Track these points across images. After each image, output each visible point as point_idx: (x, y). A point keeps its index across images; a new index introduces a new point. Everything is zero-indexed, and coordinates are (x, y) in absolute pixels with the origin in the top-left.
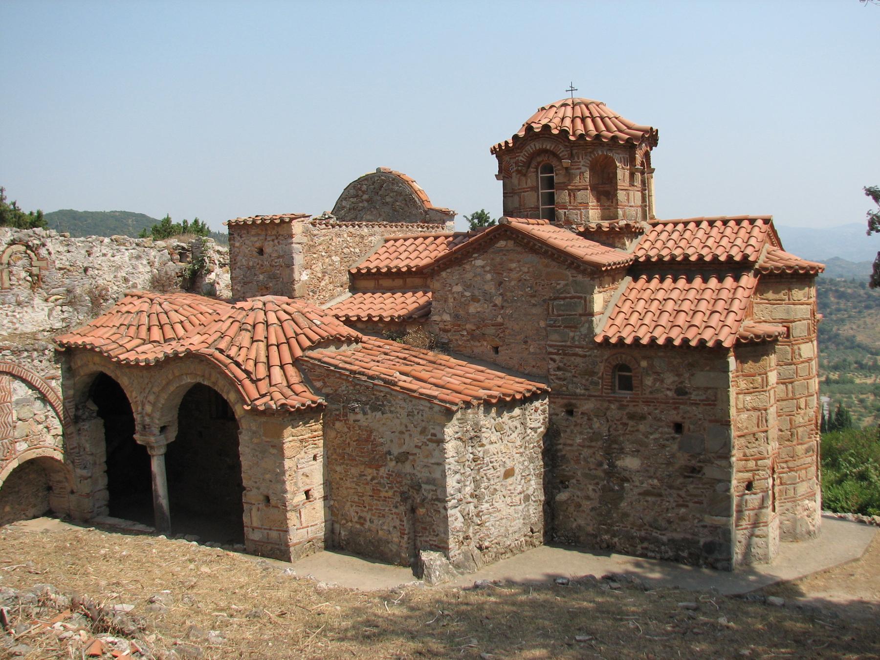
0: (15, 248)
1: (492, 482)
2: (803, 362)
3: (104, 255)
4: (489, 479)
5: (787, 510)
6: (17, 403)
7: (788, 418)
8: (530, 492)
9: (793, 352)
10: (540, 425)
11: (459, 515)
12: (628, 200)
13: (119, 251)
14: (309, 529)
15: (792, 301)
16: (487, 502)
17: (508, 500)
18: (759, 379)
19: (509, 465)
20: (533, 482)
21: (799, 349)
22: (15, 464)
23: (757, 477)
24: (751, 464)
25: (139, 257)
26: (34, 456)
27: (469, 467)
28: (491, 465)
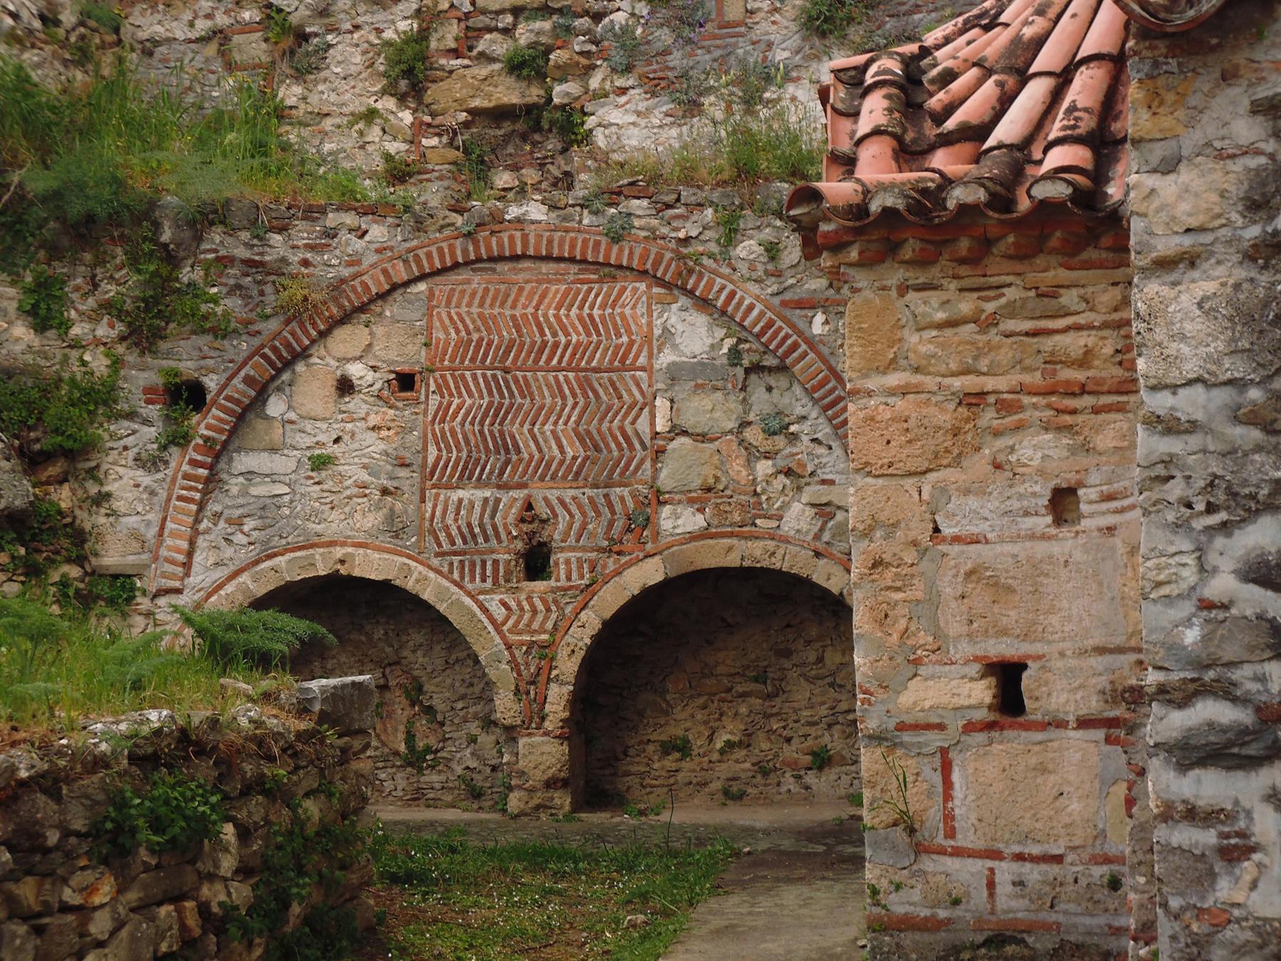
6: (675, 374)
14: (1006, 872)
17: (542, 767)
26: (733, 560)
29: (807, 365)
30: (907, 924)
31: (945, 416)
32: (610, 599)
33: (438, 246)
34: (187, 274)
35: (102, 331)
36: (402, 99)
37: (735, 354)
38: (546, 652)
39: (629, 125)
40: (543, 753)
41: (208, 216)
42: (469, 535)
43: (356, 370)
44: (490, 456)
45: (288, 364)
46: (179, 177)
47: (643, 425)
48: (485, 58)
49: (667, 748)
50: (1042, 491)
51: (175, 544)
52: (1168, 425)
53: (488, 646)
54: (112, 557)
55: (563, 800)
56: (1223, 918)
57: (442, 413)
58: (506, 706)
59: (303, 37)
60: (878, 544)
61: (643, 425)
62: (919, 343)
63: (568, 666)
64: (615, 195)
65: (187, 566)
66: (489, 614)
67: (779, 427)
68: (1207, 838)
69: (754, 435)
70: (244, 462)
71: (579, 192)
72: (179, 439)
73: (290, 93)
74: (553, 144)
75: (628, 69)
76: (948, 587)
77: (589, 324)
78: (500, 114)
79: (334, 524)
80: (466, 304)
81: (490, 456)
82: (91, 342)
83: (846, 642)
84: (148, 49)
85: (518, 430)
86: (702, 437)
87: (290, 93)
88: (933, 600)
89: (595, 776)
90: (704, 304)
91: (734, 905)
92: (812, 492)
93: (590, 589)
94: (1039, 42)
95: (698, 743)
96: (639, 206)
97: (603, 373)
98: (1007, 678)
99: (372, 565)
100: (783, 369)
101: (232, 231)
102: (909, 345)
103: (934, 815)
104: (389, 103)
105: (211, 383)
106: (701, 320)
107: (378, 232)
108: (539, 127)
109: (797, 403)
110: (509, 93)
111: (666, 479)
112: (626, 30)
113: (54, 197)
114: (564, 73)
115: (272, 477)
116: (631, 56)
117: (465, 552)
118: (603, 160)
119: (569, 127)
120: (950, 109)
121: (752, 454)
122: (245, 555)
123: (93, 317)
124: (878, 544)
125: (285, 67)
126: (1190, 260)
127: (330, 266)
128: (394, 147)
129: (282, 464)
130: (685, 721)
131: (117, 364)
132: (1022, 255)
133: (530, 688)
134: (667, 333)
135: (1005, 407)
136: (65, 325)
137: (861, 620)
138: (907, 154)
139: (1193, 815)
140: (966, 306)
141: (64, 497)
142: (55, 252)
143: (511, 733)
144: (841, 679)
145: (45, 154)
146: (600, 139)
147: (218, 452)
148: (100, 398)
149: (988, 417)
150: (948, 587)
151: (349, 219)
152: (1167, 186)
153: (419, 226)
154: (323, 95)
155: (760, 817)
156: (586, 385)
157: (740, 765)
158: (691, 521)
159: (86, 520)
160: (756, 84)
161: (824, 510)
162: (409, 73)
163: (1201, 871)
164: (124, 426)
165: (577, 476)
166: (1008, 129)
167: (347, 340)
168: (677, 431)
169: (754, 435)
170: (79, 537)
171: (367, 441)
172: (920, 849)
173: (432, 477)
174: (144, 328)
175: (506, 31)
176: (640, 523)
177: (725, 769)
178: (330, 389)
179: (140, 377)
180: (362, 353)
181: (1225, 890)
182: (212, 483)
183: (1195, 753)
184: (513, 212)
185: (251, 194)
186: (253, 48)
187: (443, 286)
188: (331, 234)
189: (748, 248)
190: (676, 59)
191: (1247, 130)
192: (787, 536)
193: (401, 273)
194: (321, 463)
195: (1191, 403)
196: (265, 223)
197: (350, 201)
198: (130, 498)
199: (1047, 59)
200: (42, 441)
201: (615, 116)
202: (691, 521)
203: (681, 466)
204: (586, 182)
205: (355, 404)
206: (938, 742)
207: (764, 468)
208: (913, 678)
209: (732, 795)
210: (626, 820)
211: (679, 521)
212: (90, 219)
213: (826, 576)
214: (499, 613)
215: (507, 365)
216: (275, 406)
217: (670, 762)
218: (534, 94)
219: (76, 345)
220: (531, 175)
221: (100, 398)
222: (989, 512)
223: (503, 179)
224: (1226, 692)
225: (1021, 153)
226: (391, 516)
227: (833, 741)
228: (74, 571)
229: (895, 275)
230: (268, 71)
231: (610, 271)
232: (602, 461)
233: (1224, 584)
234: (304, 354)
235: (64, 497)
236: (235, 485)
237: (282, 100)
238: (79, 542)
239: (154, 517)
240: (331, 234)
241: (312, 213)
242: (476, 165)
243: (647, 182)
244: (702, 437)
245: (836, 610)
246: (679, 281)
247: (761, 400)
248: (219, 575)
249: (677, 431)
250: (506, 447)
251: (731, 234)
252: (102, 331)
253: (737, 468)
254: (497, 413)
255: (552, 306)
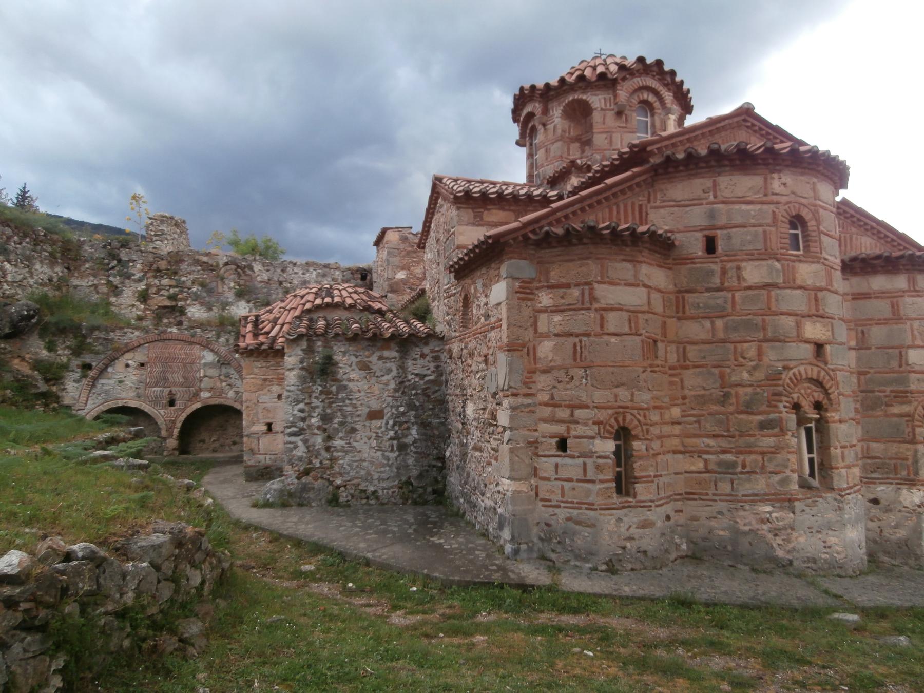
0: (228, 267)
1: (349, 419)
2: (749, 288)
3: (296, 273)
4: (345, 417)
5: (720, 513)
6: (205, 365)
7: (716, 371)
8: (409, 440)
9: (724, 272)
10: (429, 372)
11: (300, 443)
12: (611, 142)
13: (308, 271)
14: (268, 457)
15: (720, 198)
16: (341, 438)
18: (576, 292)
19: (375, 405)
20: (414, 432)
21: (739, 268)
22: (198, 405)
23: (573, 433)
24: (563, 413)
25: (324, 276)
26: (217, 403)
27: (316, 398)
28: (347, 402)
29: (234, 363)
30: (251, 466)
31: (260, 382)
32: (189, 411)
33: (151, 337)
34: (88, 341)
35: (66, 352)
36: (141, 303)
37: (218, 361)
38: (174, 422)
39: (195, 312)
40: (172, 443)
41: (93, 329)
42: (156, 397)
43: (130, 362)
44: (162, 380)
45: (113, 360)
46: (86, 320)
47: (198, 375)
48: (162, 295)
49: (200, 441)
50: (276, 395)
51: (83, 399)
52: (289, 391)
53: (161, 421)
54: (66, 402)
55: (177, 453)
56: (294, 456)
57: (151, 372)
58: (164, 433)
59: (117, 288)
60: (248, 404)
61: (198, 375)
62: (256, 370)
63: (179, 425)
64: (193, 328)
65: (86, 404)
66: (161, 414)
67: (228, 376)
68: (292, 446)
69: (222, 377)
70: (101, 381)
71: (184, 327)
72: (84, 376)
73: (113, 299)
74: (177, 314)
75: (196, 300)
76: (260, 411)
77: (186, 354)
78: (165, 307)
79: (124, 395)
80: (156, 350)
81: (162, 380)
82: (63, 354)
83: (241, 420)
84: (75, 287)
85: (169, 376)
86: (211, 378)
87: (113, 299)
88: (257, 413)
89: (184, 447)
90: (212, 351)
91: (217, 469)
92: (234, 389)
93: (184, 409)
94: (279, 318)
95: (207, 440)
96: (198, 330)
97: (189, 365)
98: (269, 426)
99: (133, 404)
100: (229, 364)
101: (101, 331)
102: (255, 370)
103: (256, 448)
104: (138, 303)
105: (94, 364)
106: (211, 354)
107: (137, 333)
108: (174, 311)
109: (232, 371)
110: (168, 303)
111: (203, 386)
112: (196, 293)
113: (56, 324)
114: (181, 300)
115: (109, 385)
116: (196, 298)
117: (155, 401)
118: (190, 319)
119: (182, 311)
120: (263, 328)
121: (222, 381)
122: (101, 402)
123: (64, 349)
124: (248, 404)
125: (111, 294)
126: (292, 369)
127: (125, 340)
128: (139, 313)
129: (111, 382)
130: (204, 435)
131: (69, 360)
132: (273, 357)
133: (170, 429)
134: (204, 356)
135: (270, 381)
136: (57, 351)
137: (244, 416)
138: (256, 336)
139: (290, 443)
140: (264, 364)
141: (54, 389)
142: (54, 335)
143: (165, 439)
144: (240, 427)
145: (52, 314)
146: (189, 314)
147: (95, 379)
148: (65, 367)
149: (268, 383)
150: (260, 411)
151: (130, 330)
152: (290, 359)
153: (147, 332)
154: (121, 300)
155: (221, 455)
156: (185, 366)
157: (217, 445)
158: (208, 395)
159: (60, 394)
160: (225, 305)
161: (237, 393)
162: (143, 297)
163: (291, 450)
164: (71, 373)
165: (182, 385)
166: (273, 334)
167: (128, 356)
168: (205, 376)
169: (222, 377)
170: (58, 397)
171: (132, 377)
172: (254, 454)
173: (147, 385)
174: (77, 352)
175: (168, 290)
176: (196, 395)
177: (213, 445)
178: (124, 366)
179: (76, 363)
180: (131, 359)
181: (294, 452)
182: (93, 386)
183: (291, 435)
184: (169, 330)
185: (105, 323)
186: (104, 289)
187: (152, 345)
188: (126, 333)
189: (222, 340)
190: (207, 299)
191: (300, 353)
192: (229, 397)
193: (142, 342)
194: (120, 382)
195: (292, 388)
196: (107, 330)
197: (129, 325)
198: (72, 389)
199: (280, 322)
200: (49, 376)
201: (193, 310)
202: (208, 395)
203: (206, 383)
204: (185, 323)
205: (129, 369)
206: (257, 436)
207: (224, 384)
208: (252, 425)
209: (215, 451)
210: (190, 456)
211: (205, 395)
212: (65, 328)
213: (237, 406)
214: (163, 414)
215: (168, 362)
216: (110, 369)
217: (201, 444)
218: (174, 303)
219: (59, 355)
220: (172, 320)
221: (65, 367)
222: (267, 398)
223: (165, 321)
224: (295, 426)
225: (274, 339)
226: (138, 394)
227: (237, 439)
228: (56, 405)
229: (252, 359)
230: (108, 295)
231: (191, 343)
232: (188, 382)
233: (295, 412)
234: (117, 359)
235: (54, 389)
236: (99, 386)
237: (13, 203)
238: (57, 399)
239: (78, 393)
240: (126, 333)
241: (121, 328)
242: (158, 318)
243: (202, 325)
244: (211, 378)
245: (239, 413)
246: (207, 346)
247: (224, 370)
248: (92, 407)
249: (205, 376)
250: (166, 379)
251: (218, 337)
252: (66, 352)
253: (218, 384)
254: (164, 372)
255: (179, 351)
